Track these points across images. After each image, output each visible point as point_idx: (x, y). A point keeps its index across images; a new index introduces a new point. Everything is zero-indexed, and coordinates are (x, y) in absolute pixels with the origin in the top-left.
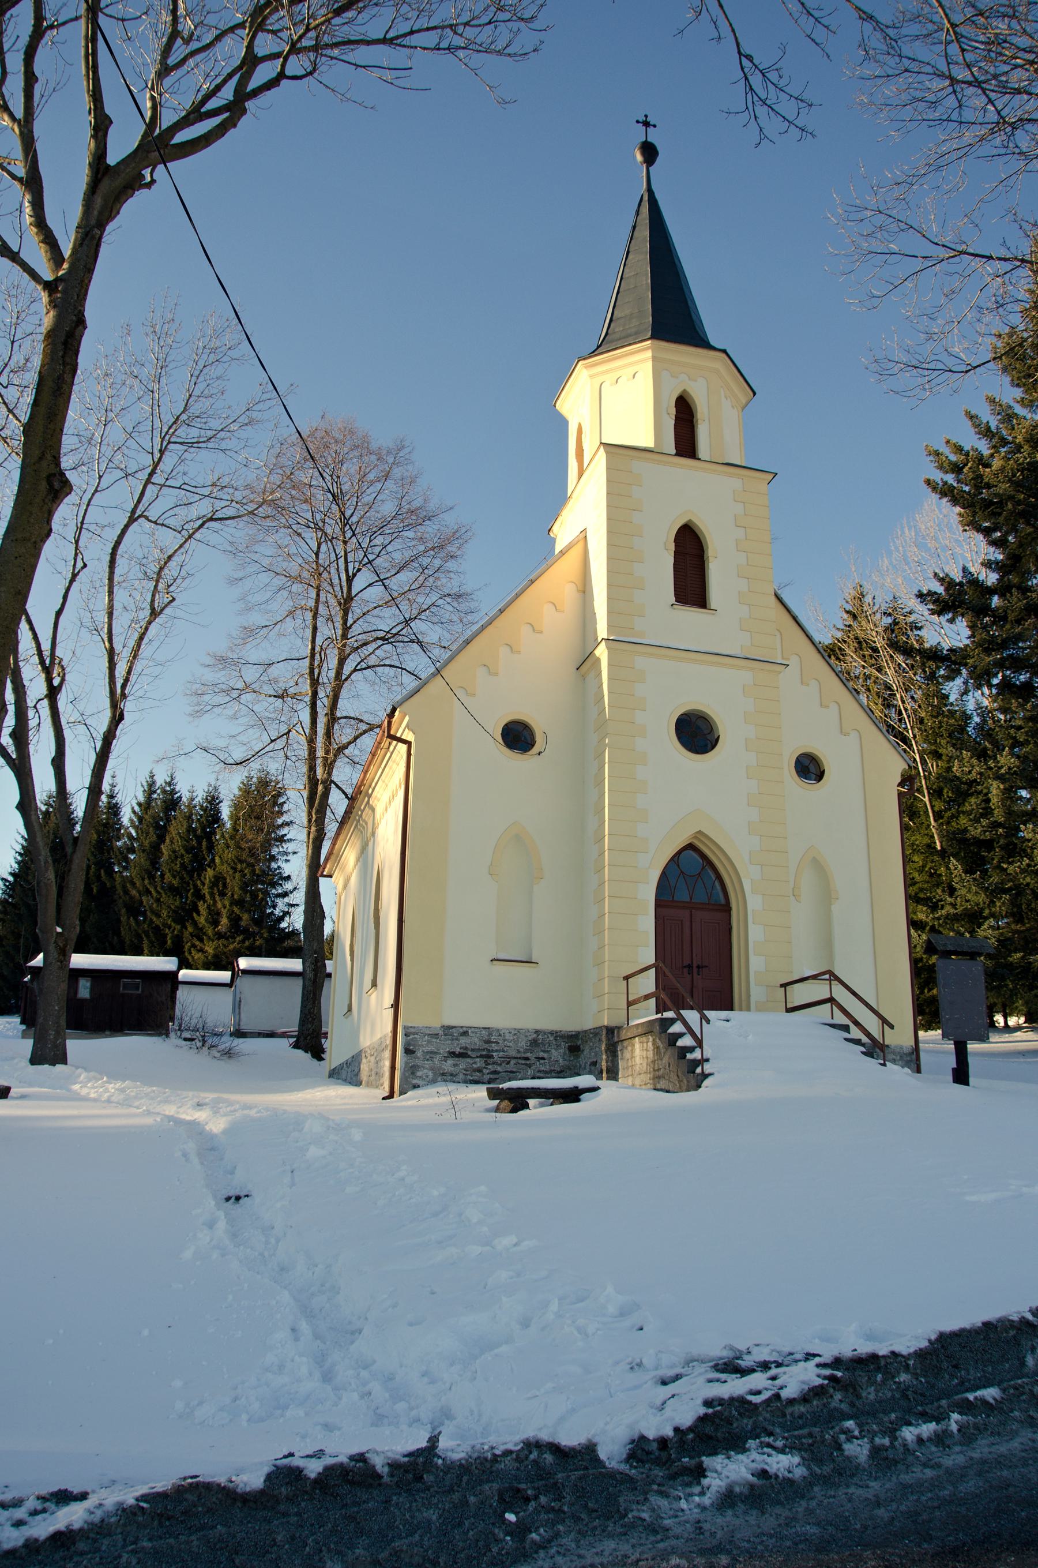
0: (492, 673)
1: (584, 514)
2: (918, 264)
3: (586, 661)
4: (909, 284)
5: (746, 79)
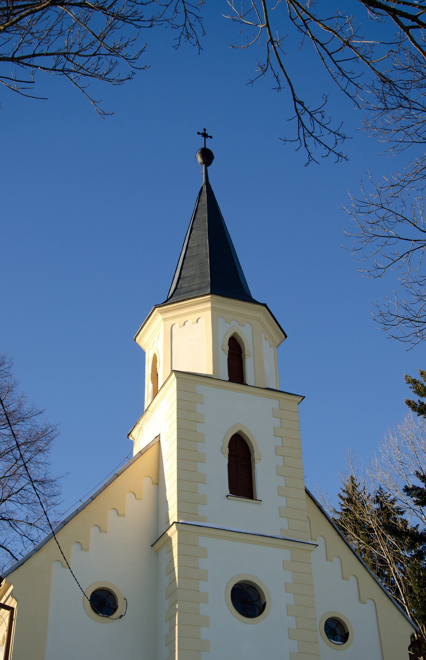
0: (84, 548)
1: (159, 423)
2: (409, 246)
3: (159, 540)
4: (403, 260)
5: (299, 118)
